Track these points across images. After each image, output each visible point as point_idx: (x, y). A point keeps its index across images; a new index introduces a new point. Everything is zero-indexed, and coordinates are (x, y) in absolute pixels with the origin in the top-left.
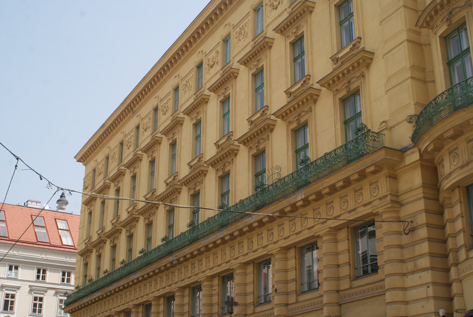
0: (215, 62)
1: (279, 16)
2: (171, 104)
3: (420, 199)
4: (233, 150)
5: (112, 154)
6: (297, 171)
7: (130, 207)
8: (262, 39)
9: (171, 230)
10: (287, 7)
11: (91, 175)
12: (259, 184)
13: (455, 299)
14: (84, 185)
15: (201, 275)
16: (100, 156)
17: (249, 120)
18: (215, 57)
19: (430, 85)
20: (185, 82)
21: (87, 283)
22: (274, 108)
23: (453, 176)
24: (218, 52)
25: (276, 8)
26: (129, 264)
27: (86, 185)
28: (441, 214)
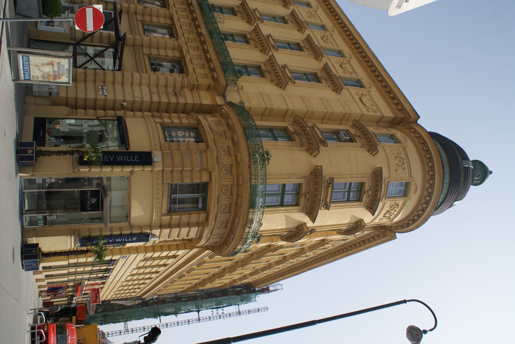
3: (194, 102)
4: (251, 21)
23: (205, 121)
25: (322, 39)
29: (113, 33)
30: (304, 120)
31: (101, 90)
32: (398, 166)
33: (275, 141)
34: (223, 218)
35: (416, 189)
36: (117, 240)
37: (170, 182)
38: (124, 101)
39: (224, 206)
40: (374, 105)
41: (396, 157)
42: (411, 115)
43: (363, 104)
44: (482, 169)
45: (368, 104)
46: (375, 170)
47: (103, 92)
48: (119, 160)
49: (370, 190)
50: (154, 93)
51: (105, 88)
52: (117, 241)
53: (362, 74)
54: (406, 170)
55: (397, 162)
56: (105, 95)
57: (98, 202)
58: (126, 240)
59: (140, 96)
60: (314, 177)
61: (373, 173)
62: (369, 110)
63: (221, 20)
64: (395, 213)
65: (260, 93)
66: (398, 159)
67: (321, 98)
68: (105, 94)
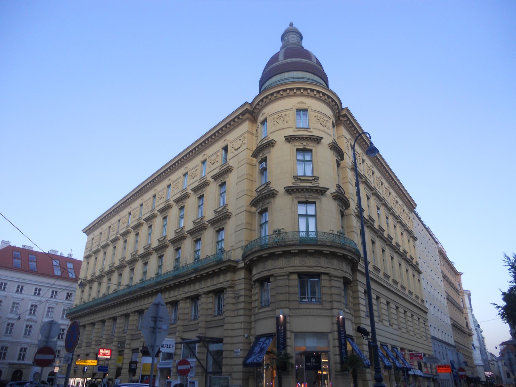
2: (116, 227)
3: (243, 283)
4: (184, 236)
5: (104, 233)
6: (260, 238)
7: (111, 264)
11: (90, 242)
13: (252, 330)
14: (86, 247)
15: (106, 317)
16: (97, 233)
17: (175, 231)
20: (146, 203)
21: (82, 303)
22: (187, 229)
23: (256, 276)
24: (126, 218)
25: (193, 178)
26: (108, 295)
27: (87, 247)
28: (251, 290)
29: (197, 345)
31: (237, 354)
35: (302, 102)
36: (342, 343)
38: (244, 336)
40: (240, 139)
41: (277, 123)
42: (245, 109)
43: (240, 148)
44: (287, 35)
45: (240, 143)
47: (238, 352)
48: (282, 341)
49: (302, 144)
50: (238, 313)
51: (235, 350)
52: (344, 342)
53: (219, 145)
54: (287, 113)
55: (280, 122)
56: (240, 350)
57: (314, 357)
58: (343, 336)
59: (240, 324)
62: (244, 143)
63: (185, 260)
64: (322, 116)
66: (278, 121)
67: (237, 183)
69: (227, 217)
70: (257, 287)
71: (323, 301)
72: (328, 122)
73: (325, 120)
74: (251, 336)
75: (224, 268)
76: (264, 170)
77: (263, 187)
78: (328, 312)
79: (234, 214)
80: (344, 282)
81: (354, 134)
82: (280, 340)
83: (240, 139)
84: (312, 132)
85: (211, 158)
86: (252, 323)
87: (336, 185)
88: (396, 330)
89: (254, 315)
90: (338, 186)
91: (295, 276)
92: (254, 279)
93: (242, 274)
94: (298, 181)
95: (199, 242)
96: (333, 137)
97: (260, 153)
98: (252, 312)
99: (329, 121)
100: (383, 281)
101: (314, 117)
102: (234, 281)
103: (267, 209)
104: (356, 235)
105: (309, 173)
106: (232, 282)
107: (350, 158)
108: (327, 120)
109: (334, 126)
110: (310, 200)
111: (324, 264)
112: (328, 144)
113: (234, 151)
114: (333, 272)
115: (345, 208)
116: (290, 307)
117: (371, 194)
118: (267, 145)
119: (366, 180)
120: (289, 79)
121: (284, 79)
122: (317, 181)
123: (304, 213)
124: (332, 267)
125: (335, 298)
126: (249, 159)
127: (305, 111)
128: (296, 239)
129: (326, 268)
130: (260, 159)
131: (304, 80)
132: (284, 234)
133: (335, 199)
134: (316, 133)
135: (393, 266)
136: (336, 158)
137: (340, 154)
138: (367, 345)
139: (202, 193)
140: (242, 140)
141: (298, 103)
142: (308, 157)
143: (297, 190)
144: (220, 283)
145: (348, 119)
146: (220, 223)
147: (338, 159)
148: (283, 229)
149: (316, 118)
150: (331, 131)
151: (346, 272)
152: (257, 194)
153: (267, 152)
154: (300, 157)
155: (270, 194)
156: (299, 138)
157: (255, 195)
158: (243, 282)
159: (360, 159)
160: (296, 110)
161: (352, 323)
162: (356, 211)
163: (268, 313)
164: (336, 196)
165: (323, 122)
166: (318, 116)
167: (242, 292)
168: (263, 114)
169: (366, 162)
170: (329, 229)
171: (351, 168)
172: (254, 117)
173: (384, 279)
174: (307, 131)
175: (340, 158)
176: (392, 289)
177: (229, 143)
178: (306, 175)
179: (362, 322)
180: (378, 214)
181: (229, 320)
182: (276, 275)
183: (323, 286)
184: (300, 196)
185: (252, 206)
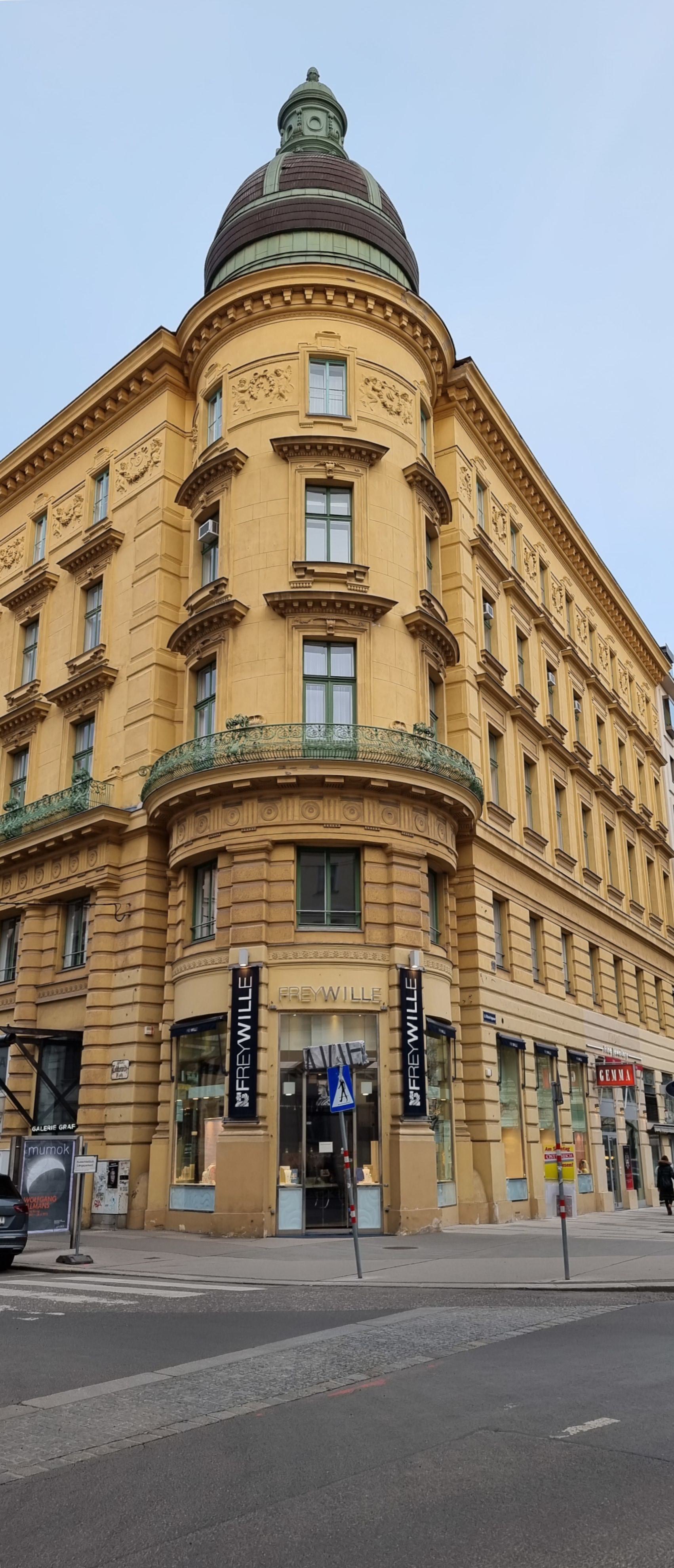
0: (72, 515)
1: (12, 579)
8: (103, 531)
9: (202, 716)
10: (24, 570)
12: (80, 772)
18: (74, 506)
19: (177, 725)
22: (46, 688)
23: (178, 853)
25: (9, 567)
28: (166, 895)
30: (183, 622)
32: (271, 391)
33: (216, 700)
34: (374, 813)
35: (328, 334)
37: (293, 928)
39: (347, 812)
40: (144, 446)
43: (142, 474)
45: (143, 459)
46: (279, 455)
47: (122, 1069)
49: (324, 465)
50: (126, 960)
51: (115, 1064)
55: (260, 394)
60: (290, 611)
61: (285, 459)
62: (155, 460)
64: (390, 382)
65: (125, 727)
67: (133, 584)
68: (127, 1065)
69: (103, 683)
70: (181, 885)
71: (366, 923)
72: (406, 400)
73: (397, 394)
74: (160, 1024)
75: (89, 830)
76: (210, 544)
77: (206, 593)
78: (380, 953)
79: (123, 673)
80: (429, 869)
81: (489, 443)
82: (240, 1033)
83: (144, 446)
84: (354, 429)
85: (60, 507)
86: (166, 988)
87: (421, 592)
88: (588, 1008)
89: (172, 964)
90: (427, 597)
91: (290, 854)
92: (174, 861)
93: (141, 849)
94: (306, 579)
95: (23, 757)
96: (420, 450)
97: (200, 494)
98: (167, 957)
99: (411, 396)
100: (554, 873)
101: (363, 383)
102: (119, 869)
103: (215, 661)
104: (476, 740)
105: (340, 554)
106: (112, 871)
107: (472, 517)
108: (404, 395)
109: (425, 417)
110: (339, 634)
111: (372, 818)
112: (404, 470)
113: (126, 485)
114: (397, 842)
115: (443, 662)
116: (268, 942)
117: (532, 626)
118: (217, 465)
119: (519, 585)
120: (291, 254)
121: (278, 256)
122: (362, 578)
123: (323, 672)
124: (395, 827)
125: (400, 914)
126: (168, 509)
127: (338, 361)
128: (293, 747)
129: (377, 829)
130: (200, 511)
131: (339, 261)
132: (258, 731)
133: (413, 635)
134: (366, 434)
135: (588, 832)
136: (424, 513)
137: (439, 503)
138: (492, 1046)
139: (33, 610)
140: (150, 451)
141: (317, 335)
142: (339, 505)
143: (303, 603)
144: (80, 875)
145: (473, 397)
146: (84, 700)
147: (432, 516)
148: (257, 717)
149: (371, 384)
150: (414, 428)
151: (436, 843)
152: (190, 615)
153: (219, 487)
154: (317, 504)
155: (223, 613)
156: (314, 447)
157: (184, 616)
158: (145, 871)
159: (504, 523)
160: (311, 357)
161: (453, 985)
162: (480, 671)
163: (209, 958)
164: (417, 624)
165: (391, 400)
166: (375, 379)
167: (141, 901)
168: (213, 367)
169: (523, 531)
170: (393, 721)
171: (473, 547)
172: (186, 380)
173: (557, 867)
174: (341, 425)
175: (438, 515)
176: (579, 895)
177: (112, 461)
178: (332, 560)
179: (481, 985)
180: (550, 685)
181: (100, 979)
182: (234, 848)
183: (367, 880)
184: (311, 623)
185: (173, 650)
